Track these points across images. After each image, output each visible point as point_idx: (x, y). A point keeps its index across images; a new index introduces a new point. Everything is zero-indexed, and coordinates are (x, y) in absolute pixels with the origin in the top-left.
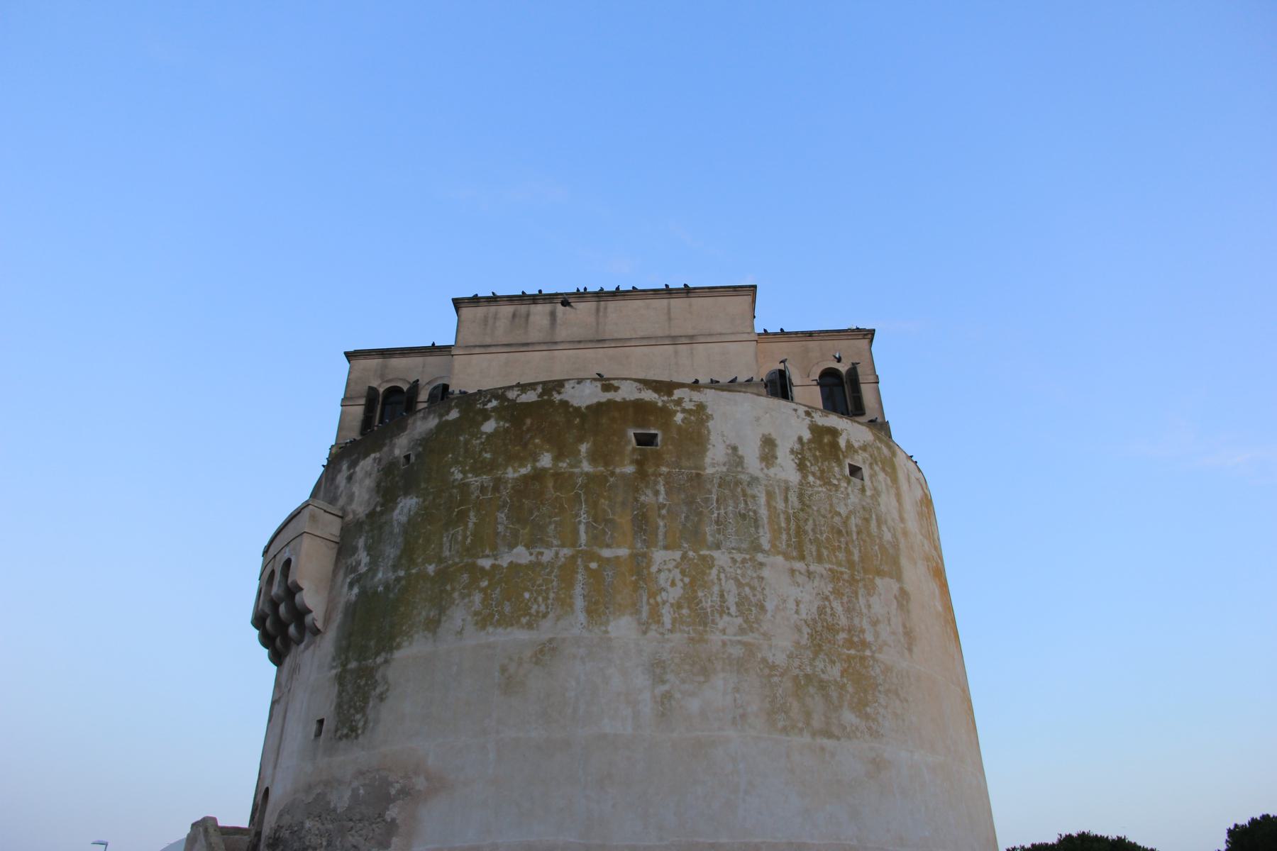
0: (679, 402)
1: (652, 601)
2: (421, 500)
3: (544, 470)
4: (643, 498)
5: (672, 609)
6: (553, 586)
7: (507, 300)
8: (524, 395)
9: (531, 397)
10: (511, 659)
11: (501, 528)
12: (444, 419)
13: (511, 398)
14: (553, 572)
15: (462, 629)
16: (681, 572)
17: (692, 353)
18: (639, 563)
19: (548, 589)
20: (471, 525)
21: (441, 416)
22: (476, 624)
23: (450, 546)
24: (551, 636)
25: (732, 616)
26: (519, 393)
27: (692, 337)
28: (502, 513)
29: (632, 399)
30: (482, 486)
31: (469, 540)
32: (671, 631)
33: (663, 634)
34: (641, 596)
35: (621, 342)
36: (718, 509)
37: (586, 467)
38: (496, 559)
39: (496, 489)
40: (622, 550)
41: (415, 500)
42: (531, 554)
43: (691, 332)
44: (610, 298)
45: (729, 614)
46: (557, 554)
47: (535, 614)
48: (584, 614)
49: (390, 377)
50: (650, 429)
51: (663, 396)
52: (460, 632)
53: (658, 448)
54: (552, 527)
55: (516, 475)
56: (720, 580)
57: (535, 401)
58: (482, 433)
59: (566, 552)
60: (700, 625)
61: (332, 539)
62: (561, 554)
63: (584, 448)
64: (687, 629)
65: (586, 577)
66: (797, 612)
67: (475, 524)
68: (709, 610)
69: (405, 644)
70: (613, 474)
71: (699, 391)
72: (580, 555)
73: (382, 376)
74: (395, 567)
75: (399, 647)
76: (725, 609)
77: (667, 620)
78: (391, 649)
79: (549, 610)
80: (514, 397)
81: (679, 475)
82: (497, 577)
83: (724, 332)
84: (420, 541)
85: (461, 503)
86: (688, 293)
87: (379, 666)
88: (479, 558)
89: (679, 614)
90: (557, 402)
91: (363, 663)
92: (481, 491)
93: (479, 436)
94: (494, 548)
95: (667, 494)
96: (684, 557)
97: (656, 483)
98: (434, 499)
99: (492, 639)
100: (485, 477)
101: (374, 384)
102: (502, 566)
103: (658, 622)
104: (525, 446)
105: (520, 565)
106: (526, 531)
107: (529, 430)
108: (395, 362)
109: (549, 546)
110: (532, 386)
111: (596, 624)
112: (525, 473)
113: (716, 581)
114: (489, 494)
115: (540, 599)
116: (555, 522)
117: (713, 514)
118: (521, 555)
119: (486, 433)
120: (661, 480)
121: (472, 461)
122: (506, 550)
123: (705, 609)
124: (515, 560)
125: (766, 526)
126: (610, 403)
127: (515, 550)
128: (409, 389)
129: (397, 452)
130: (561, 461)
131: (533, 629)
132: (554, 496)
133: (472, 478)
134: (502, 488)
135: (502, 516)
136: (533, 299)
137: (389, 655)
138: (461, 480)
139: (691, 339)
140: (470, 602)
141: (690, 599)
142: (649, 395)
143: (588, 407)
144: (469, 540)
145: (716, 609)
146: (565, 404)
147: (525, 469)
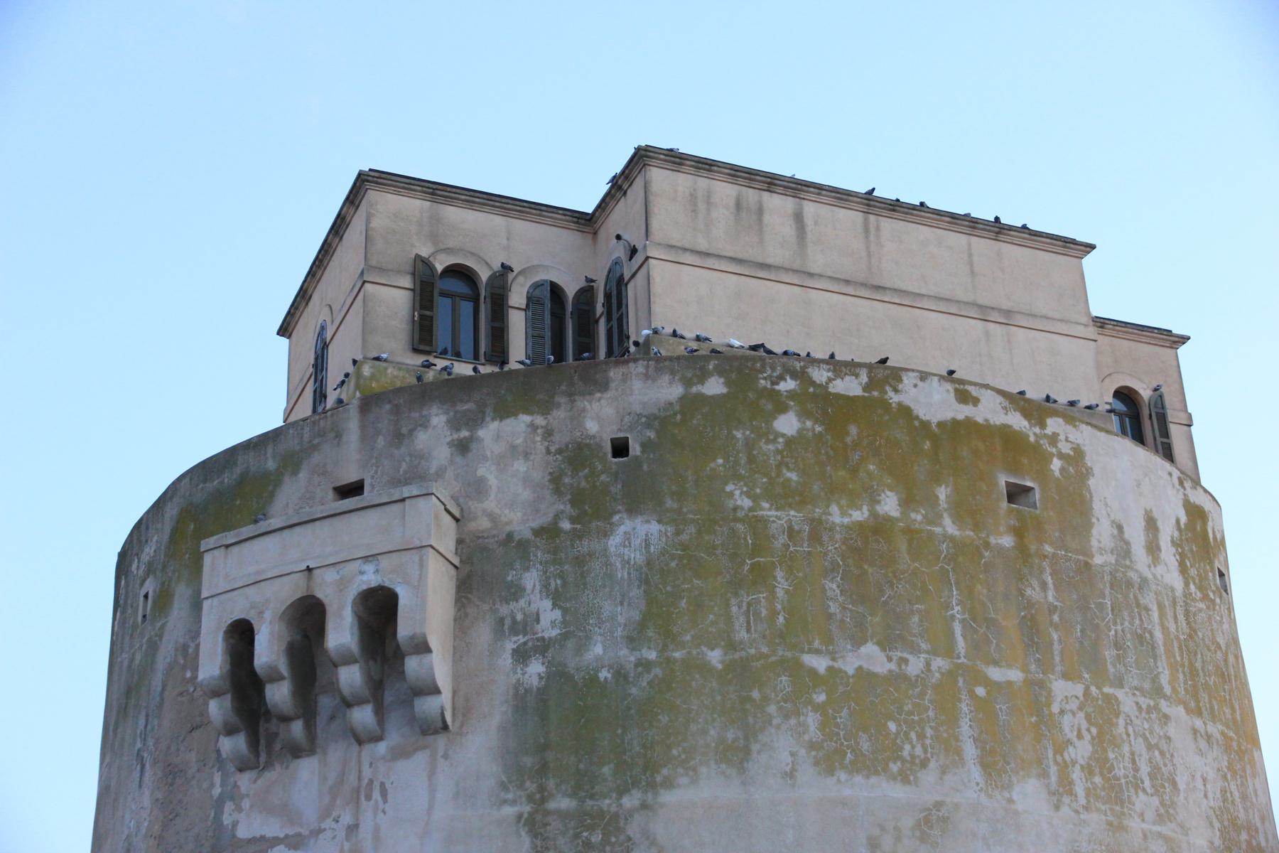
0: (1054, 439)
1: (1059, 758)
2: (671, 529)
3: (888, 519)
4: (1029, 592)
5: (1083, 774)
6: (928, 716)
7: (729, 175)
8: (838, 381)
9: (850, 386)
10: (883, 829)
11: (834, 608)
12: (694, 390)
13: (818, 382)
14: (926, 694)
15: (793, 770)
16: (1086, 718)
17: (1009, 341)
18: (1036, 693)
19: (921, 720)
20: (780, 593)
21: (688, 383)
22: (817, 763)
23: (748, 623)
24: (938, 798)
25: (1147, 794)
26: (830, 374)
27: (1008, 313)
28: (832, 580)
29: (998, 423)
30: (791, 529)
31: (781, 619)
32: (1086, 808)
33: (1077, 812)
34: (1046, 748)
35: (908, 298)
36: (1115, 623)
37: (949, 526)
38: (834, 659)
39: (815, 537)
40: (1013, 671)
41: (655, 527)
42: (890, 660)
43: (1006, 305)
44: (885, 213)
45: (1144, 790)
46: (928, 665)
47: (908, 758)
48: (979, 767)
49: (450, 244)
50: (1024, 479)
51: (1035, 426)
52: (791, 774)
53: (1038, 512)
54: (916, 619)
55: (846, 520)
56: (1128, 735)
57: (858, 396)
58: (778, 435)
59: (939, 663)
60: (1117, 804)
61: (451, 560)
62: (934, 667)
63: (942, 493)
64: (1103, 808)
65: (972, 708)
66: (1206, 796)
67: (787, 592)
68: (1123, 781)
69: (684, 780)
70: (987, 545)
71: (1075, 426)
72: (960, 672)
73: (433, 237)
74: (633, 641)
75: (669, 784)
76: (1139, 782)
77: (1079, 789)
78: (652, 786)
79: (929, 755)
80: (824, 380)
81: (1067, 561)
82: (841, 689)
83: (1050, 314)
84: (683, 603)
85: (757, 550)
86: (998, 233)
87: (630, 814)
88: (803, 651)
89: (1091, 783)
90: (894, 405)
91: (589, 802)
92: (790, 537)
93: (771, 437)
94: (828, 639)
95: (1056, 589)
96: (1087, 693)
97: (1042, 571)
98: (699, 533)
99: (847, 792)
100: (792, 513)
101: (425, 252)
102: (846, 673)
103: (1071, 794)
104: (854, 471)
105: (874, 675)
106: (877, 619)
107: (856, 445)
108: (454, 214)
109: (915, 650)
110: (851, 367)
111: (997, 786)
112: (860, 519)
113: (1125, 737)
114: (805, 545)
115: (913, 735)
116: (919, 611)
117: (1110, 631)
118: (872, 658)
119: (783, 435)
120: (1045, 564)
121: (765, 480)
122: (849, 647)
123: (1119, 779)
124: (865, 666)
125: (1163, 657)
126: (969, 423)
127: (863, 649)
128: (493, 278)
129: (592, 426)
130: (913, 510)
131: (909, 783)
132: (911, 568)
133: (770, 509)
134: (825, 538)
135: (832, 587)
136: (769, 183)
137: (650, 795)
138: (751, 509)
139: (1007, 317)
140: (799, 724)
141: (1099, 764)
142: (1017, 421)
143: (940, 424)
144: (781, 619)
145: (1130, 780)
146: (905, 411)
147: (858, 513)
